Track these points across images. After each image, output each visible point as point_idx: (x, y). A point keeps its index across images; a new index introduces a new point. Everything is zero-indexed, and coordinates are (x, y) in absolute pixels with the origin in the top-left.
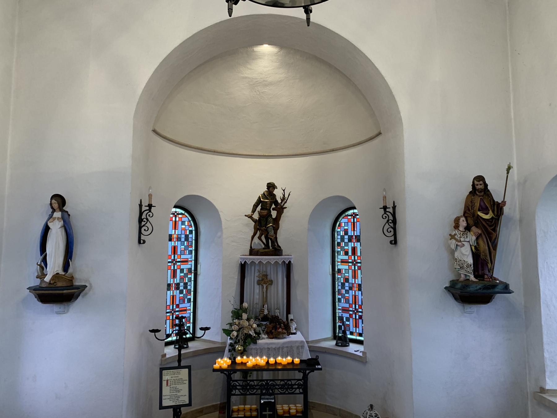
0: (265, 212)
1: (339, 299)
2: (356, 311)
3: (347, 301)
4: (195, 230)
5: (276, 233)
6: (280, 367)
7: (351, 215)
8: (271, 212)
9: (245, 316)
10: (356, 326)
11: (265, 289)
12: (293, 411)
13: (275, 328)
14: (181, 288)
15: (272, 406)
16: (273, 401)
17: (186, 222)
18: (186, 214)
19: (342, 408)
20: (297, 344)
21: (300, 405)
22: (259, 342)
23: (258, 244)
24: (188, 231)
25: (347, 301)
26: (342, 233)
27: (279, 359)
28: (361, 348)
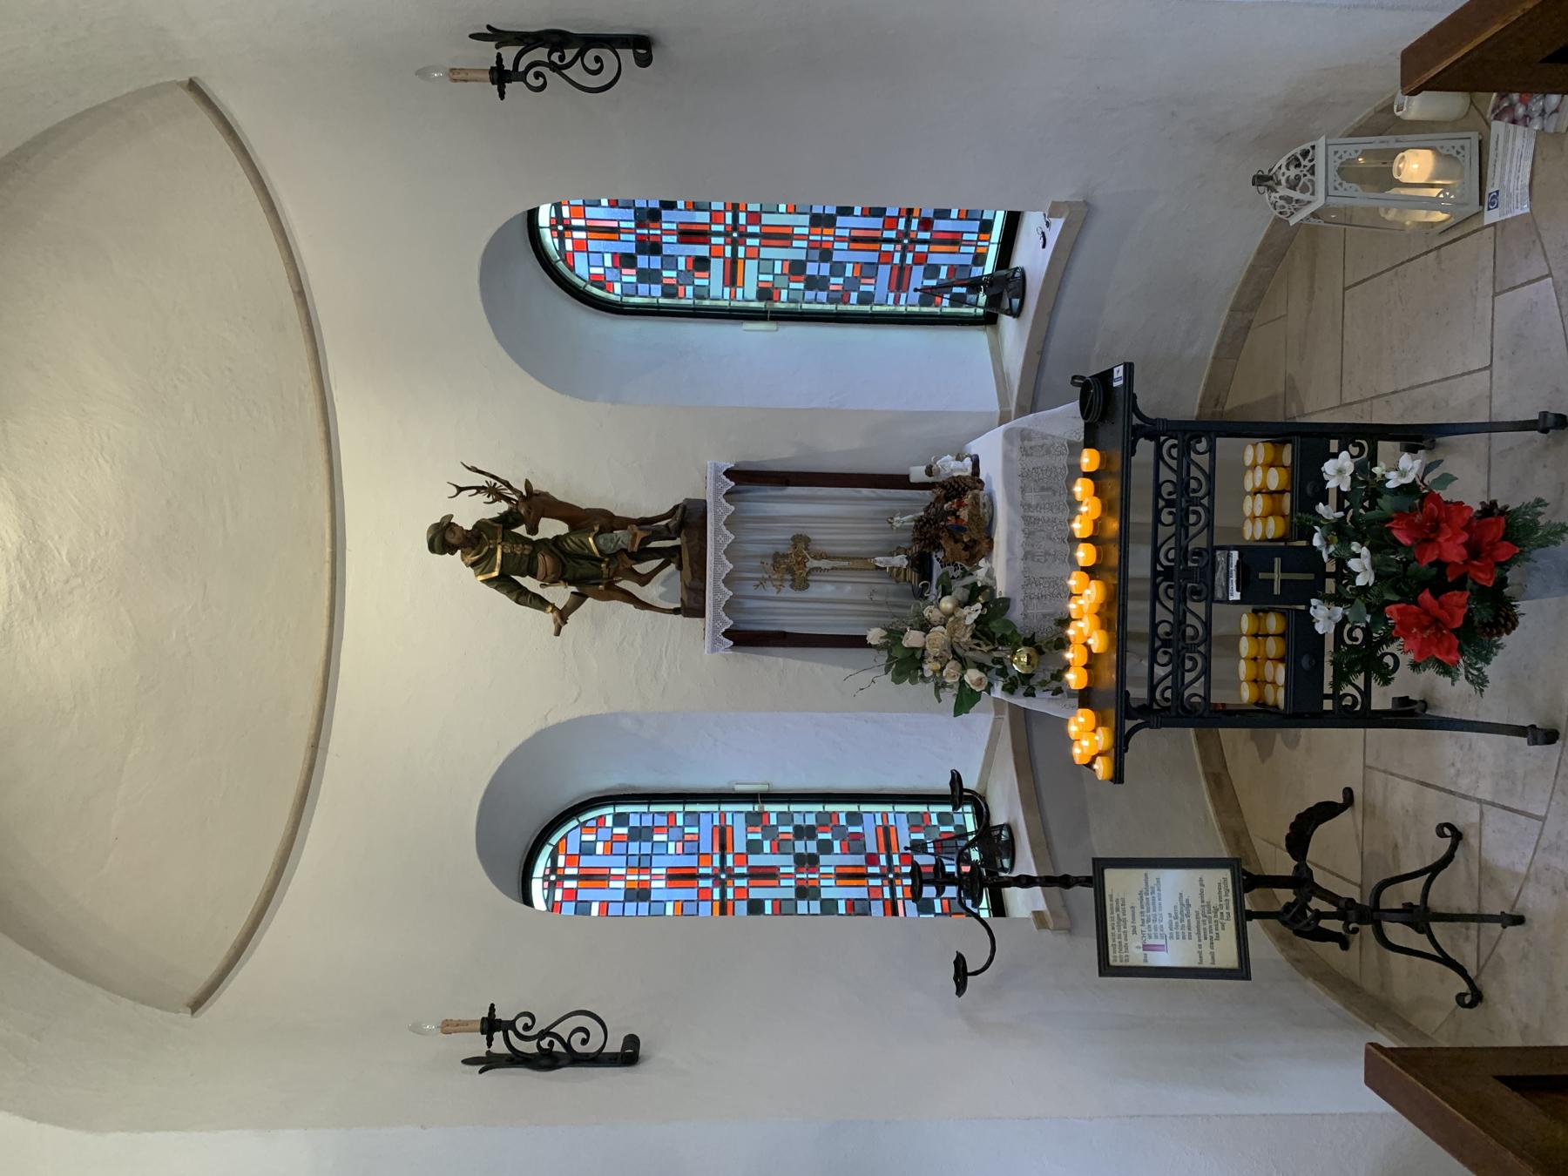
0: (544, 562)
1: (861, 302)
2: (906, 241)
3: (868, 270)
4: (615, 804)
5: (624, 523)
6: (1113, 526)
7: (561, 237)
8: (544, 541)
9: (913, 638)
10: (954, 240)
11: (823, 564)
12: (1275, 479)
13: (955, 533)
14: (812, 847)
15: (1254, 558)
16: (1235, 555)
17: (585, 838)
18: (554, 840)
19: (1230, 303)
20: (1016, 454)
21: (1249, 452)
22: (1001, 589)
23: (663, 587)
24: (617, 830)
25: (868, 270)
26: (630, 276)
27: (1080, 527)
28: (1032, 224)
